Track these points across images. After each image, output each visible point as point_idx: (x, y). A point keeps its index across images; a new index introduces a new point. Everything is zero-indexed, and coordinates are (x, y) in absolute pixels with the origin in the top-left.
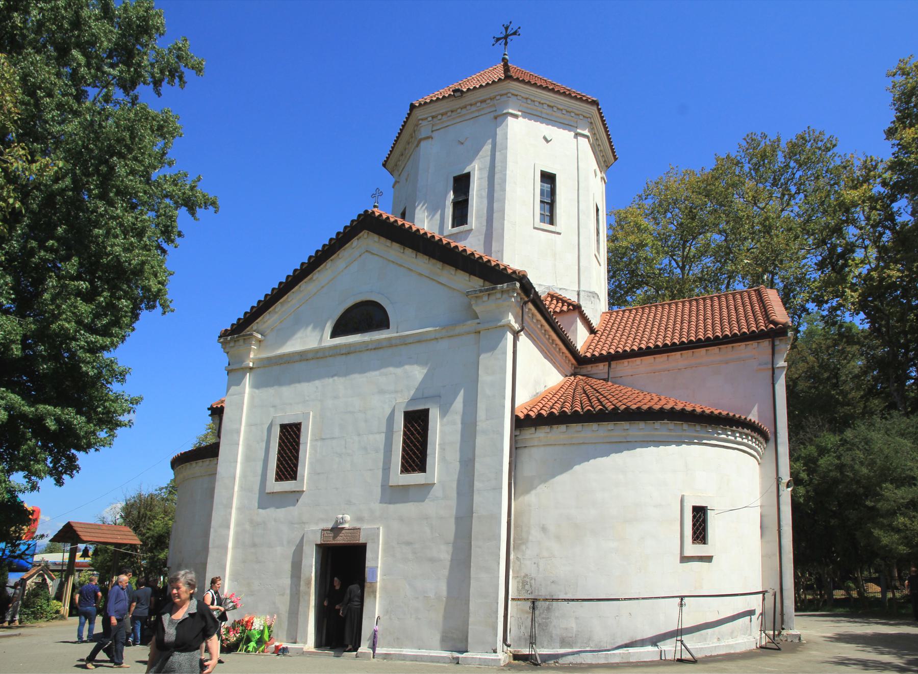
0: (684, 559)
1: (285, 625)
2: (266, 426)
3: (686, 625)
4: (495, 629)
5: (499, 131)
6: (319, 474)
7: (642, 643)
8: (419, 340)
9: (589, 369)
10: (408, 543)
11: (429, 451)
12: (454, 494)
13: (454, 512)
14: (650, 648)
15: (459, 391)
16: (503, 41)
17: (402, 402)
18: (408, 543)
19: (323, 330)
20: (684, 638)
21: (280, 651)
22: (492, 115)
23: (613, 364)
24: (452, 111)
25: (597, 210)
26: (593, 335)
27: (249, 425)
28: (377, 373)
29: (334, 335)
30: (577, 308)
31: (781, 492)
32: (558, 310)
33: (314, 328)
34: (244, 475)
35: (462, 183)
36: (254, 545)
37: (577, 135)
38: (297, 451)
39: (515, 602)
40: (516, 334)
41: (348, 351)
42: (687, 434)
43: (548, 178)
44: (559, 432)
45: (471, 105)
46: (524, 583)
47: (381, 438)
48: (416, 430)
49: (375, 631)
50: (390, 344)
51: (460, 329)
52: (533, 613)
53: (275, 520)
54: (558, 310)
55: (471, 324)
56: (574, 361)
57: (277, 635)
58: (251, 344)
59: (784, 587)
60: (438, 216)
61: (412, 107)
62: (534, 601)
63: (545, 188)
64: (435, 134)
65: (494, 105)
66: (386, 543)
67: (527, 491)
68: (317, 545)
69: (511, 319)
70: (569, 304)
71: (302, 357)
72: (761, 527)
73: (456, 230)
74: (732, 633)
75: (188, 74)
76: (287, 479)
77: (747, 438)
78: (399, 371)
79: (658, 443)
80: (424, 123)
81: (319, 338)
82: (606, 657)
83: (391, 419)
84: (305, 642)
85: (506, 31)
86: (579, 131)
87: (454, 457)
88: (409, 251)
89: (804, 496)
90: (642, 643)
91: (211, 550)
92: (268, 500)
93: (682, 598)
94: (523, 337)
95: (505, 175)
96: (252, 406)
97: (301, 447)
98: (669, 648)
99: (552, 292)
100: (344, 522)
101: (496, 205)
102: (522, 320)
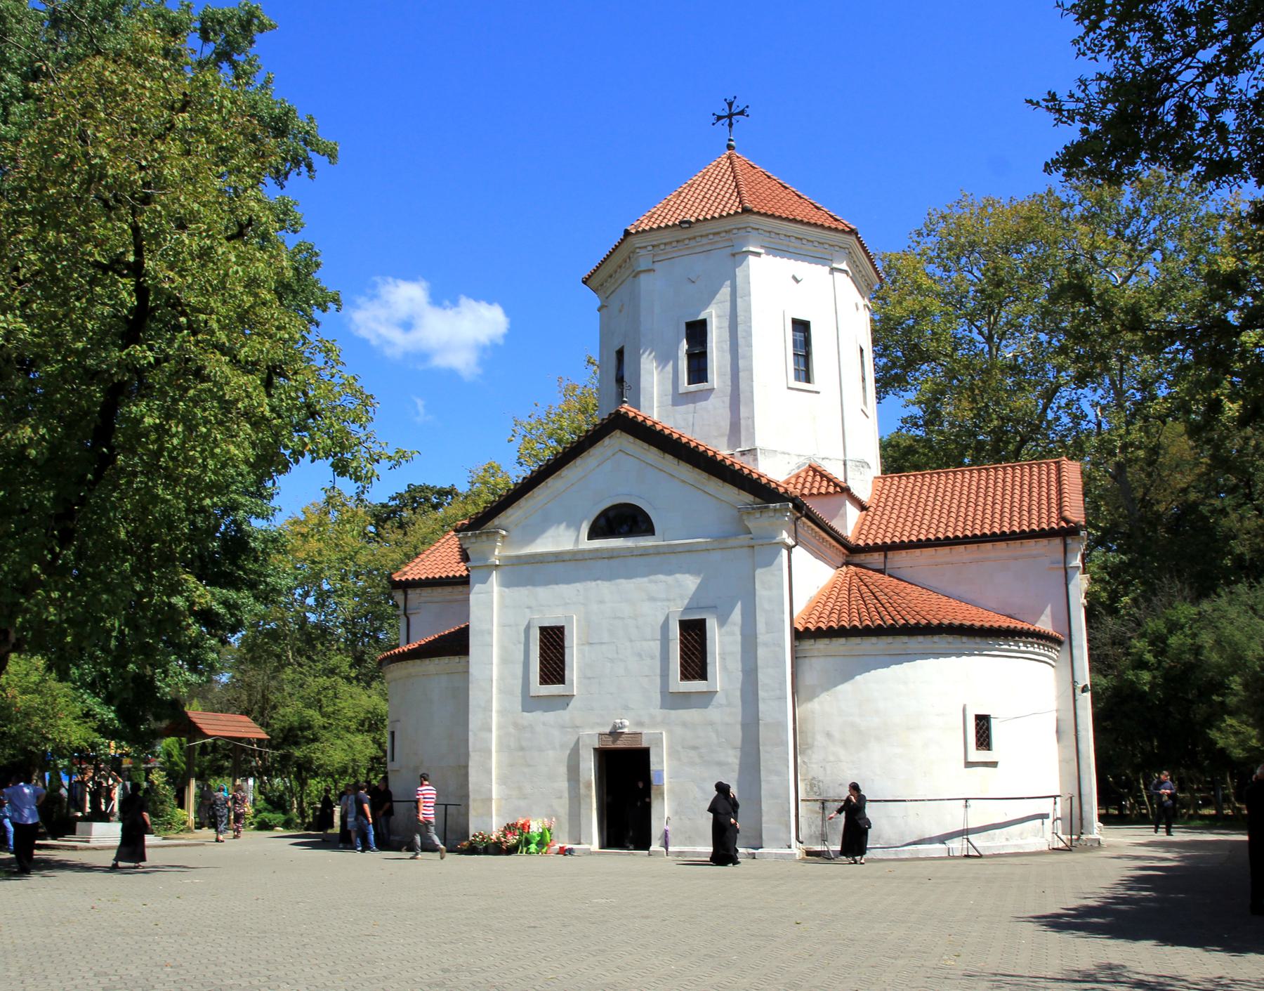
0: (969, 764)
1: (566, 826)
2: (522, 628)
3: (970, 826)
4: (789, 827)
5: (739, 272)
6: (589, 678)
7: (930, 840)
8: (690, 550)
9: (861, 558)
10: (695, 748)
11: (709, 660)
12: (738, 702)
13: (740, 719)
14: (938, 846)
15: (735, 605)
16: (726, 121)
17: (676, 610)
18: (695, 748)
19: (578, 530)
20: (970, 837)
21: (563, 851)
22: (729, 251)
23: (890, 554)
24: (678, 241)
25: (862, 350)
26: (864, 512)
27: (503, 626)
28: (645, 579)
29: (593, 534)
30: (846, 491)
31: (1077, 697)
32: (823, 490)
33: (568, 526)
34: (502, 678)
35: (697, 332)
36: (522, 749)
37: (833, 270)
38: (563, 655)
39: (804, 803)
40: (790, 549)
41: (611, 555)
42: (967, 646)
43: (802, 327)
44: (839, 644)
45: (701, 236)
46: (812, 786)
47: (656, 646)
48: (693, 638)
49: (666, 831)
50: (657, 551)
51: (732, 542)
52: (823, 813)
53: (544, 724)
54: (823, 490)
55: (744, 539)
56: (845, 551)
57: (558, 837)
58: (495, 541)
59: (1083, 792)
60: (670, 367)
61: (627, 233)
62: (823, 802)
63: (798, 338)
64: (657, 266)
65: (730, 240)
66: (670, 747)
67: (810, 698)
68: (595, 749)
69: (785, 535)
70: (836, 485)
71: (558, 557)
72: (1057, 732)
73: (694, 387)
74: (1021, 834)
75: (318, 160)
76: (554, 683)
77: (1033, 646)
78: (670, 579)
79: (937, 655)
80: (643, 252)
81: (574, 538)
82: (896, 853)
83: (665, 627)
84: (591, 843)
85: (730, 109)
86: (835, 265)
87: (736, 666)
88: (669, 457)
89: (1150, 683)
90: (930, 840)
91: (472, 754)
92: (531, 703)
93: (967, 800)
94: (798, 552)
95: (750, 327)
96: (503, 606)
97: (567, 651)
98: (957, 846)
99: (814, 465)
100: (623, 727)
101: (741, 363)
102: (796, 537)
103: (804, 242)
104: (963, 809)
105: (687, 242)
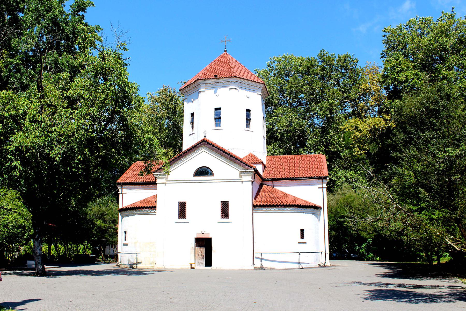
23: (274, 182)
31: (362, 286)
80: (202, 85)
103: (250, 86)
104: (299, 255)
105: (216, 83)
